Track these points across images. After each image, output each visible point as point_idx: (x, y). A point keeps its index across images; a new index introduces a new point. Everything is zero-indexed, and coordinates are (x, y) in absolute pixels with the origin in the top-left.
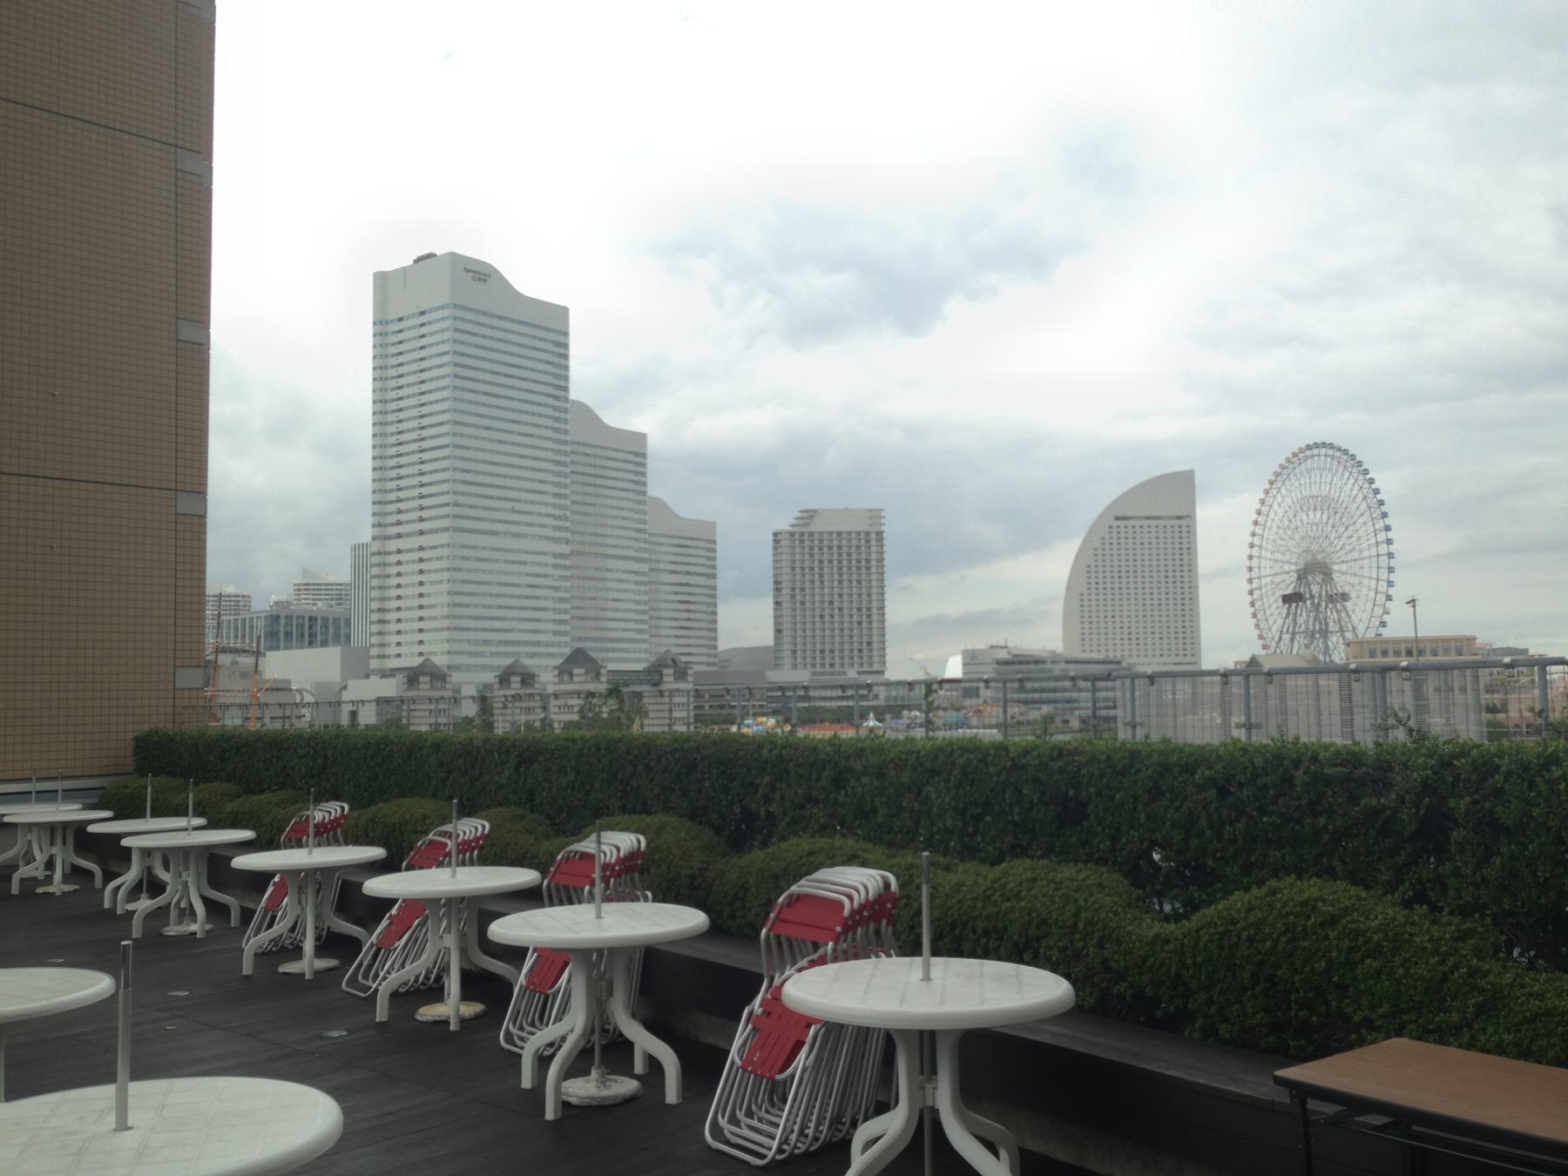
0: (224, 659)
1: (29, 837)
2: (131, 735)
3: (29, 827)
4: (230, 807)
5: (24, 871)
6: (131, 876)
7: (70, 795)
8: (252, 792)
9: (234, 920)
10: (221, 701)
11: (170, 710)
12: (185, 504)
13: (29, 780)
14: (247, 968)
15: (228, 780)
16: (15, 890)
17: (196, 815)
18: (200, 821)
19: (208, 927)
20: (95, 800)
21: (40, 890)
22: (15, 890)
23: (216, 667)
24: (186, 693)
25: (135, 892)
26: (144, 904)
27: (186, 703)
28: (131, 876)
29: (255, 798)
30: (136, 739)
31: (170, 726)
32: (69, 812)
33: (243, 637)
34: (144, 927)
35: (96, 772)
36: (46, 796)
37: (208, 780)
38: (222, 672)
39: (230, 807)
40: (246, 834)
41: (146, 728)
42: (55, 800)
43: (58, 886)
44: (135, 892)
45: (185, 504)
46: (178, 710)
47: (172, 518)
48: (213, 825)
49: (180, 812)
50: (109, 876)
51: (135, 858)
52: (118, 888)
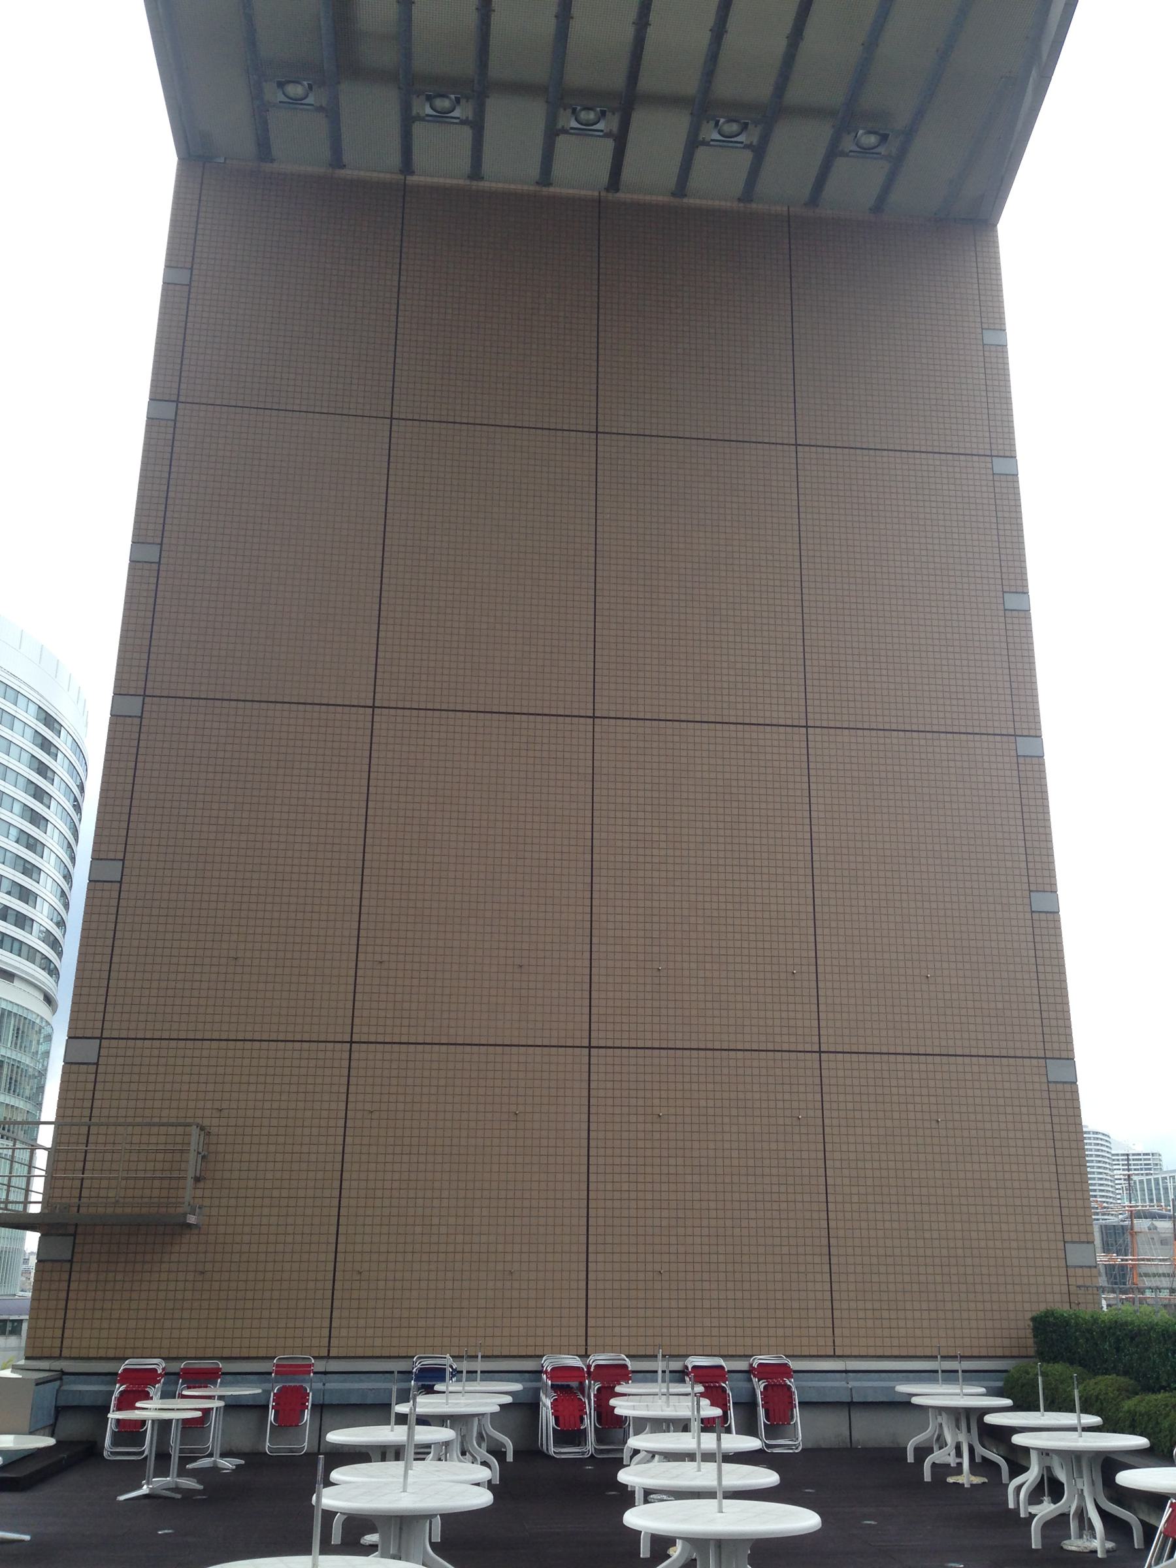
0: (1142, 1224)
1: (939, 1420)
2: (1029, 1315)
3: (940, 1410)
4: (1128, 1404)
5: (939, 1456)
6: (1031, 1476)
7: (971, 1376)
8: (1153, 1390)
9: (1138, 1543)
10: (1143, 1270)
11: (1065, 1289)
12: (1055, 1071)
13: (934, 1357)
14: (1036, 1543)
15: (1126, 1373)
16: (927, 1477)
17: (1085, 1410)
18: (1095, 1420)
19: (1110, 1545)
20: (1000, 1384)
21: (950, 1480)
22: (927, 1477)
23: (1133, 1234)
24: (1079, 1271)
25: (1035, 1496)
26: (1046, 1509)
27: (1080, 1282)
28: (1031, 1476)
29: (1152, 1397)
30: (1033, 1319)
31: (1066, 1307)
32: (971, 1396)
33: (1159, 1200)
34: (1043, 1537)
35: (1000, 1352)
36: (950, 1376)
37: (1106, 1372)
38: (1140, 1239)
39: (1128, 1404)
40: (1140, 1442)
41: (1043, 1307)
42: (935, 1381)
43: (966, 1478)
44: (1035, 1496)
45: (1055, 1071)
46: (1073, 1289)
47: (1045, 1087)
48: (1110, 1426)
49: (1066, 1406)
50: (1014, 1474)
51: (1034, 1457)
52: (1019, 1488)
